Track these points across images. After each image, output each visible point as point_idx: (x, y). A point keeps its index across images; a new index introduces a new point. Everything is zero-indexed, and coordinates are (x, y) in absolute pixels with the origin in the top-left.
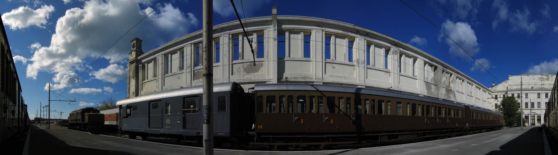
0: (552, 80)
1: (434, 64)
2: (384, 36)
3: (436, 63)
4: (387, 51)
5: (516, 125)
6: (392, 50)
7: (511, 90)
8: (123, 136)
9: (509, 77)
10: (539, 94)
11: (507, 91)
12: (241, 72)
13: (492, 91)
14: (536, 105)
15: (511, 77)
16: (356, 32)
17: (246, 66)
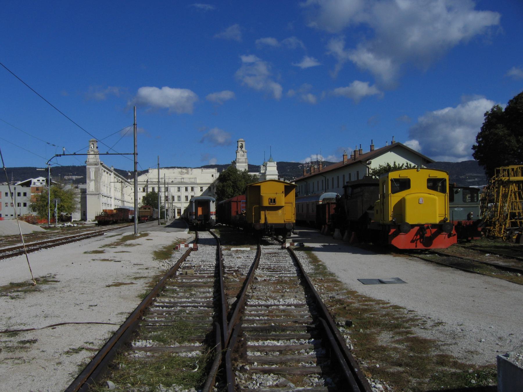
10: (179, 188)
14: (176, 199)
15: (151, 170)
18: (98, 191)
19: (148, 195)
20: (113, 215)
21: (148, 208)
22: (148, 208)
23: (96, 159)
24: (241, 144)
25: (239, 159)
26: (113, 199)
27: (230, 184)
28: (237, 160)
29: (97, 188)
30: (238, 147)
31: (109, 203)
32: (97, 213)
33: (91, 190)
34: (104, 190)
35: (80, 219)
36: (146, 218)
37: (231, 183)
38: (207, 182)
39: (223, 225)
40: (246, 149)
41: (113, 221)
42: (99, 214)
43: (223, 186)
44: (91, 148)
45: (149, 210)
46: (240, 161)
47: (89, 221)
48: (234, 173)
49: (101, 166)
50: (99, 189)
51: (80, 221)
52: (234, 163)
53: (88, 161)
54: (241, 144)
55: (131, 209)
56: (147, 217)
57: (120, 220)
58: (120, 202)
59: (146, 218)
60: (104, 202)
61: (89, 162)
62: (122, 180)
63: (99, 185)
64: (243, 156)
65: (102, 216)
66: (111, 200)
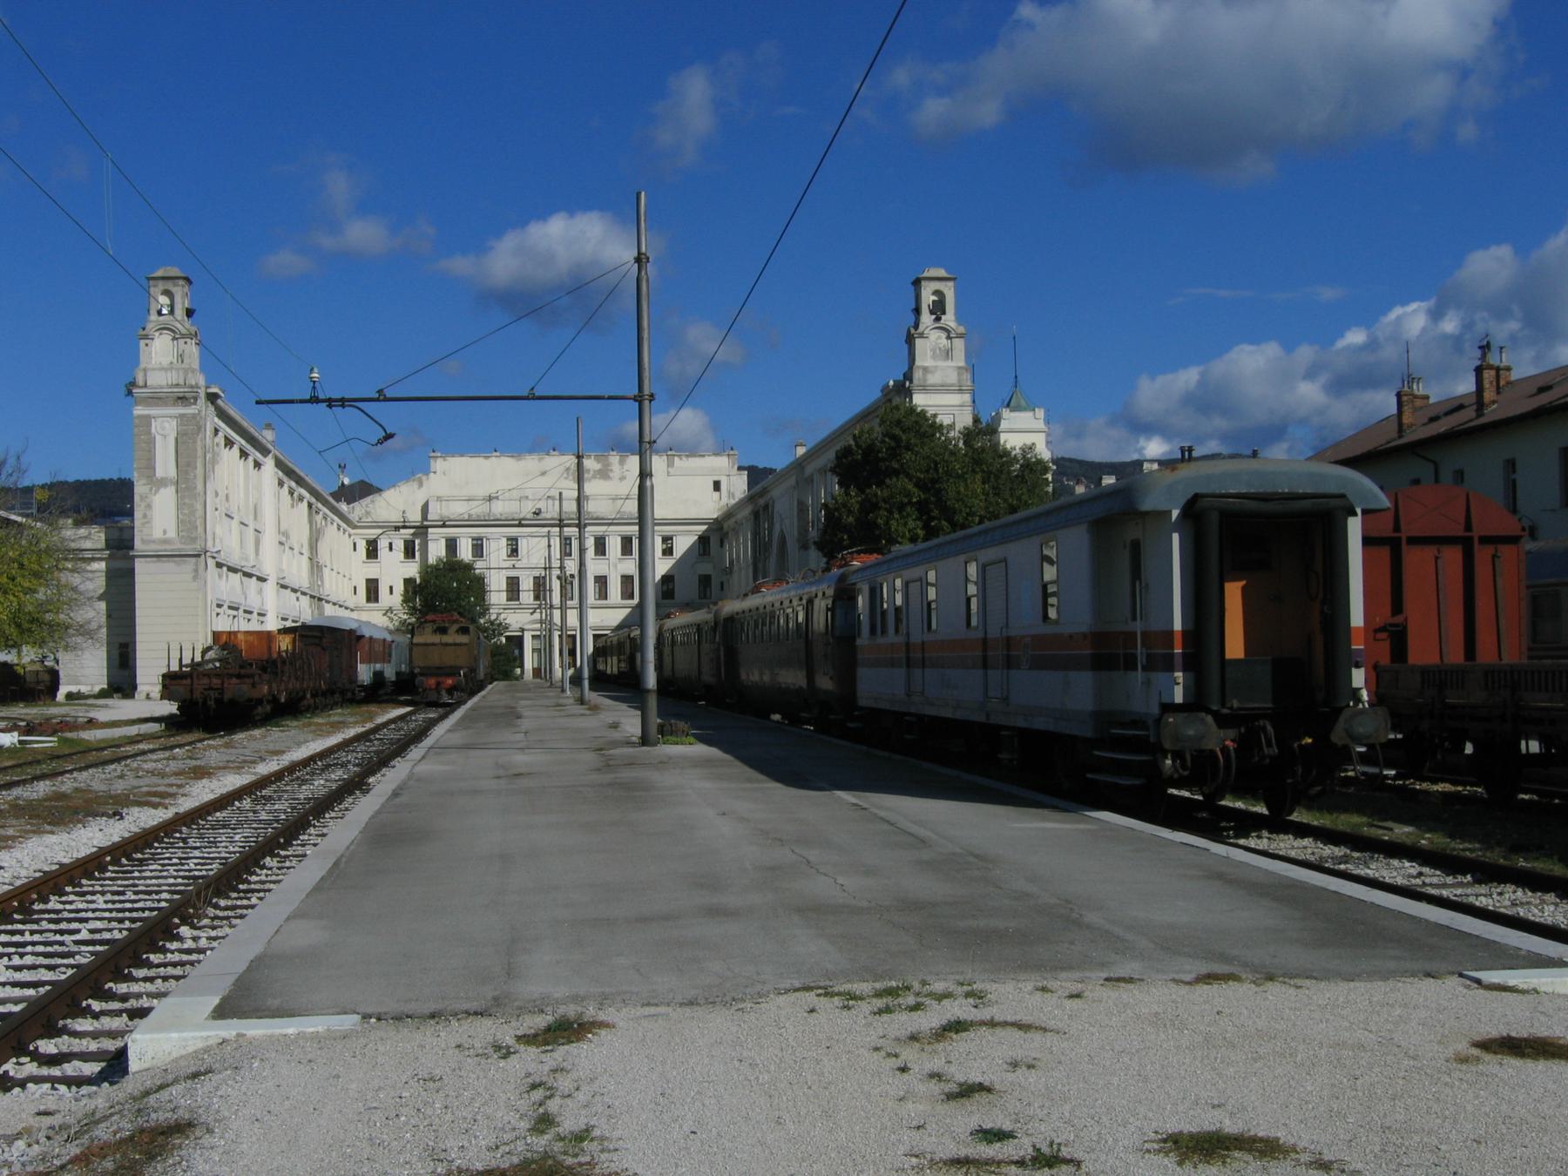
0: (622, 478)
4: (1385, 553)
8: (1263, 844)
9: (432, 461)
13: (354, 517)
15: (439, 460)
18: (194, 540)
19: (429, 572)
20: (274, 662)
21: (455, 627)
22: (455, 627)
23: (186, 371)
24: (936, 292)
25: (925, 369)
26: (270, 588)
27: (909, 495)
28: (917, 375)
29: (191, 520)
30: (917, 311)
31: (253, 602)
32: (175, 655)
33: (157, 534)
34: (227, 539)
35: (102, 684)
36: (450, 682)
37: (910, 487)
38: (694, 513)
39: (1401, 782)
40: (959, 318)
41: (274, 700)
42: (187, 660)
43: (869, 506)
44: (160, 313)
45: (464, 639)
46: (932, 379)
47: (148, 697)
48: (924, 435)
49: (211, 409)
50: (200, 530)
51: (103, 694)
52: (903, 388)
53: (141, 383)
54: (936, 292)
55: (367, 635)
56: (452, 671)
57: (314, 696)
58: (305, 600)
59: (450, 682)
60: (227, 598)
61: (146, 386)
62: (313, 500)
63: (199, 507)
64: (948, 354)
65: (207, 674)
66: (260, 592)
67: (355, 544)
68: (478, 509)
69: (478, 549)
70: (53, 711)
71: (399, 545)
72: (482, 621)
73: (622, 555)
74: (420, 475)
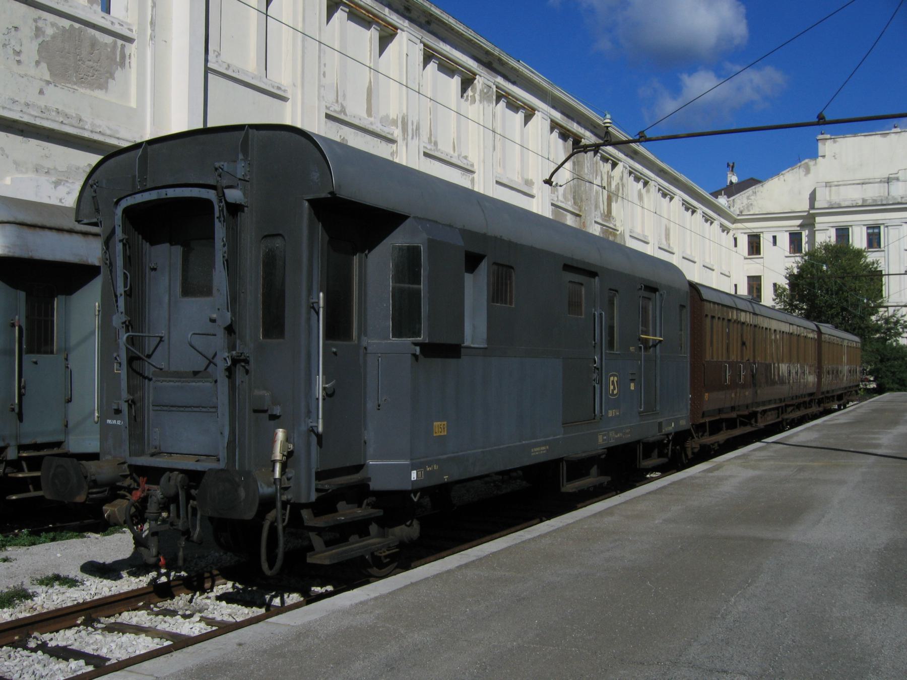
1: (575, 127)
2: (469, 33)
3: (579, 123)
5: (873, 385)
6: (479, 82)
7: (834, 210)
9: (820, 144)
11: (813, 216)
12: (22, 58)
13: (735, 211)
15: (828, 143)
16: (402, 9)
17: (50, 31)
67: (735, 239)
68: (873, 192)
69: (874, 240)
70: (111, 508)
71: (784, 240)
72: (873, 318)
73: (749, 254)
74: (806, 161)
